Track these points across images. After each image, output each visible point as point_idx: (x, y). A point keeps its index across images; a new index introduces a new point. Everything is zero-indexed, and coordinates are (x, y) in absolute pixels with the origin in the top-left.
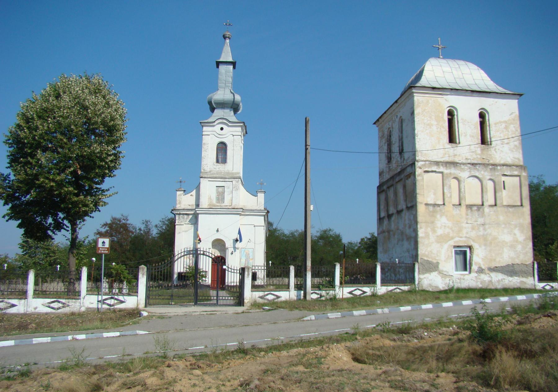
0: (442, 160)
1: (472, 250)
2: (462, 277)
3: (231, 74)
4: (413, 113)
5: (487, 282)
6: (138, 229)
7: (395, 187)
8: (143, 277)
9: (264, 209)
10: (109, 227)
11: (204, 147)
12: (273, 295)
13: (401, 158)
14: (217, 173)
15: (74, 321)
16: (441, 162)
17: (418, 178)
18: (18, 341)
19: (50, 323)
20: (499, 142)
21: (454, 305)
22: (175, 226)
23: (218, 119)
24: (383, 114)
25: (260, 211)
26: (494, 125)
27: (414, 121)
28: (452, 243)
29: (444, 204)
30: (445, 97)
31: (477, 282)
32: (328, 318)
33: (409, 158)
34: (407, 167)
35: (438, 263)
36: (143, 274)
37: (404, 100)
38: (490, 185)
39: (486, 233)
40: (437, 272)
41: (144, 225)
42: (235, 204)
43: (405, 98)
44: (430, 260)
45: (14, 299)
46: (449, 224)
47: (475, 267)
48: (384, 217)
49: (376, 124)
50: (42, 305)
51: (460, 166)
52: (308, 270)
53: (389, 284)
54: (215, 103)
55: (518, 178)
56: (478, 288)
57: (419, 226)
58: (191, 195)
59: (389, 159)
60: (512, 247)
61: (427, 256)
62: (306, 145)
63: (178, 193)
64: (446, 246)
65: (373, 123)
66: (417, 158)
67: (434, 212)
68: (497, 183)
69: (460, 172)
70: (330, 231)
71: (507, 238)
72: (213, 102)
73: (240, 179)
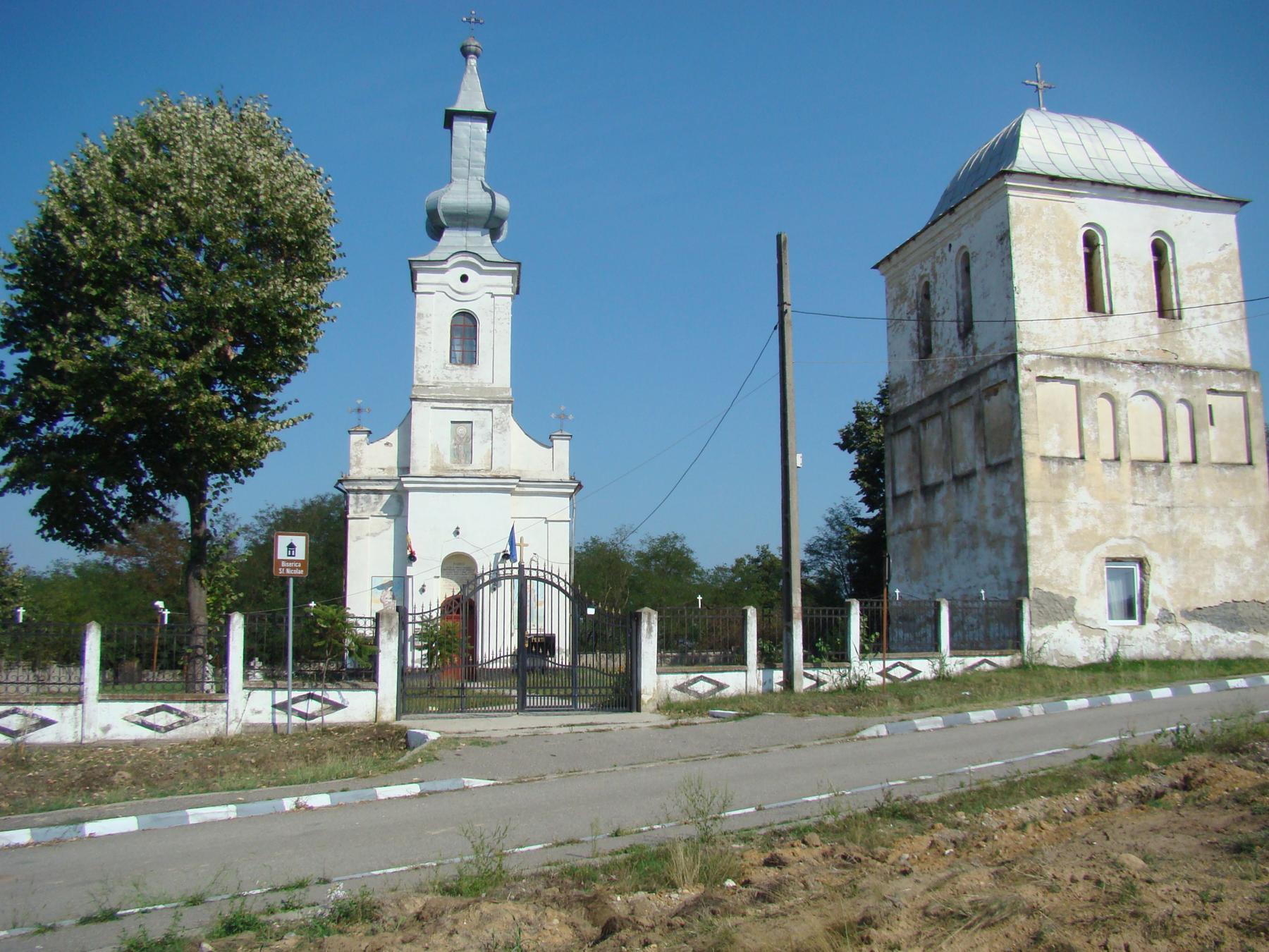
0: (1074, 351)
1: (1147, 567)
2: (1126, 632)
3: (484, 144)
4: (1004, 237)
5: (1180, 643)
7: (947, 417)
8: (389, 639)
11: (420, 324)
12: (709, 681)
13: (964, 348)
15: (235, 759)
16: (1073, 356)
17: (1024, 394)
18: (147, 818)
19: (168, 768)
20: (1197, 312)
21: (1175, 693)
22: (345, 521)
24: (908, 242)
26: (1186, 273)
27: (1010, 256)
28: (1102, 551)
29: (1082, 458)
30: (1078, 200)
31: (1159, 644)
32: (917, 731)
33: (991, 347)
34: (988, 368)
35: (1073, 599)
36: (390, 633)
37: (976, 206)
38: (1181, 413)
39: (1175, 528)
40: (1070, 622)
42: (500, 466)
43: (979, 200)
44: (1055, 591)
45: (46, 704)
46: (1096, 505)
47: (1153, 610)
48: (908, 494)
49: (881, 266)
50: (124, 719)
51: (1116, 368)
52: (794, 615)
53: (967, 652)
54: (445, 215)
55: (1240, 399)
56: (1161, 658)
57: (1028, 510)
58: (387, 444)
59: (925, 350)
60: (1233, 560)
61: (1048, 584)
62: (781, 303)
63: (354, 438)
64: (1089, 559)
65: (874, 264)
66: (1019, 346)
67: (1062, 476)
68: (1196, 409)
69: (1115, 381)
71: (1221, 540)
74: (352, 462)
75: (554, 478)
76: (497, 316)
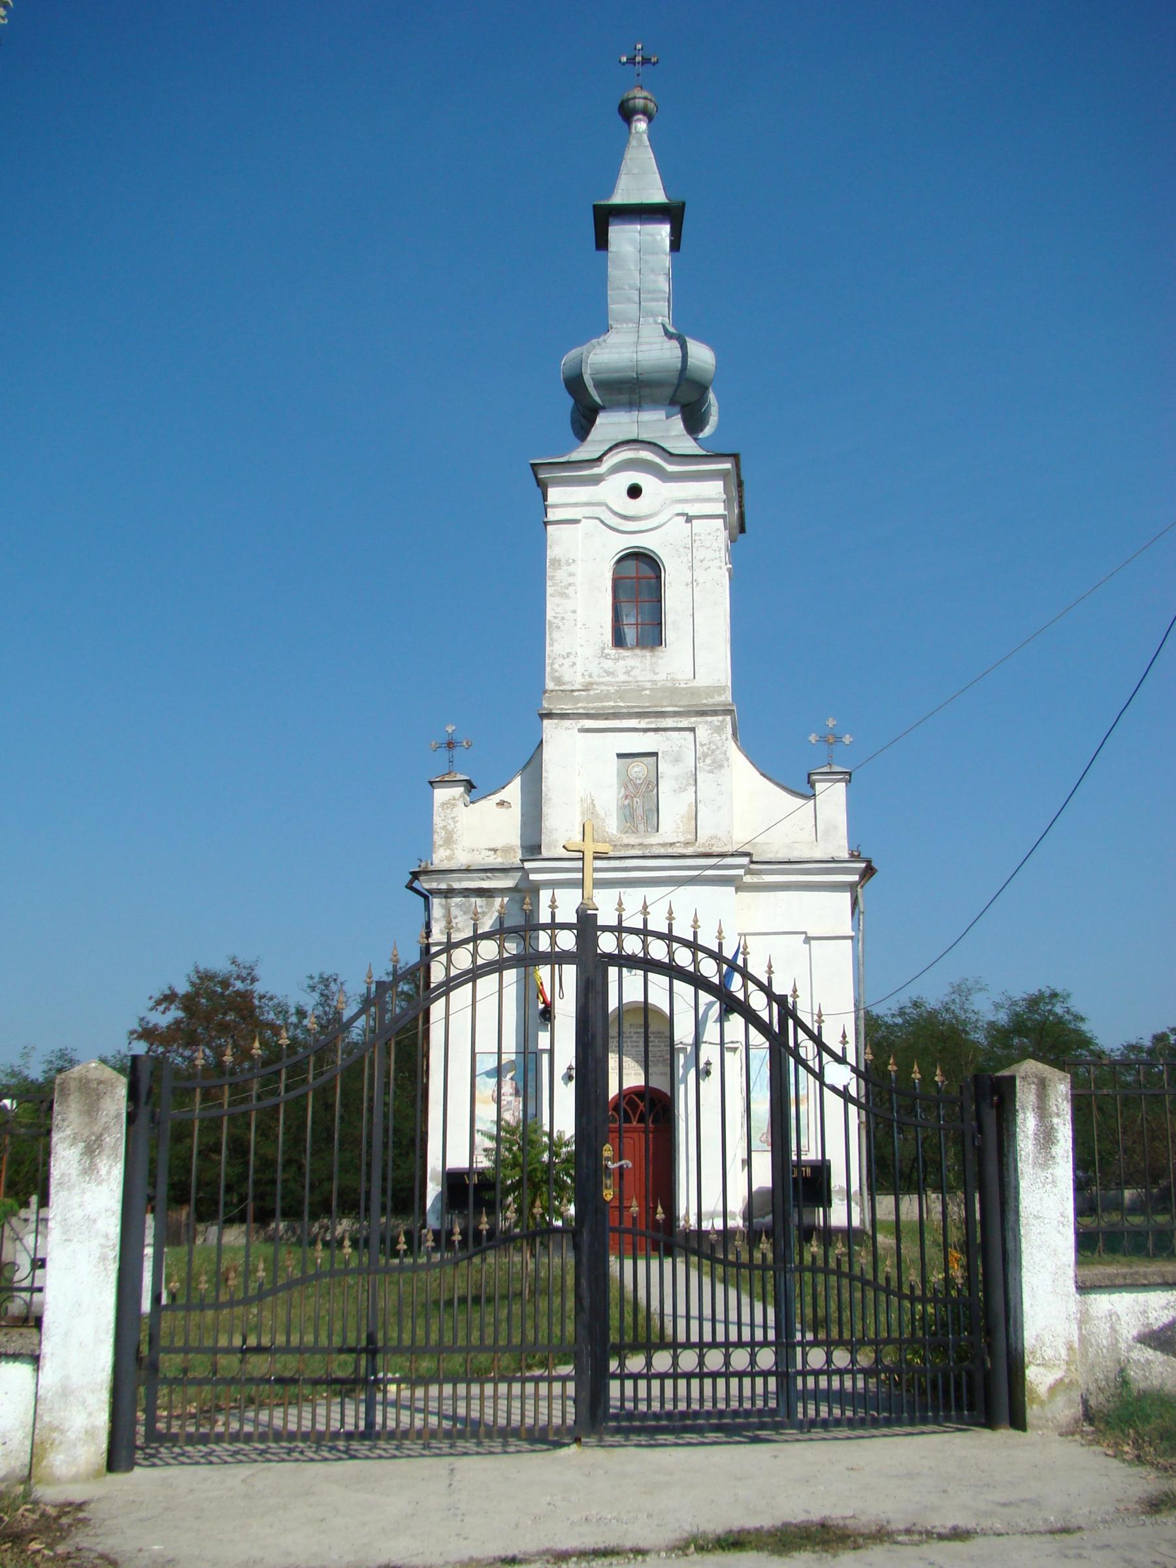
6: (292, 1010)
8: (89, 1170)
9: (852, 855)
10: (186, 1009)
11: (555, 579)
14: (621, 694)
23: (610, 449)
25: (830, 864)
36: (92, 1149)
41: (316, 996)
42: (712, 833)
58: (501, 803)
63: (441, 795)
70: (1054, 1001)
72: (587, 379)
73: (728, 718)
74: (438, 839)
75: (818, 855)
76: (699, 555)
